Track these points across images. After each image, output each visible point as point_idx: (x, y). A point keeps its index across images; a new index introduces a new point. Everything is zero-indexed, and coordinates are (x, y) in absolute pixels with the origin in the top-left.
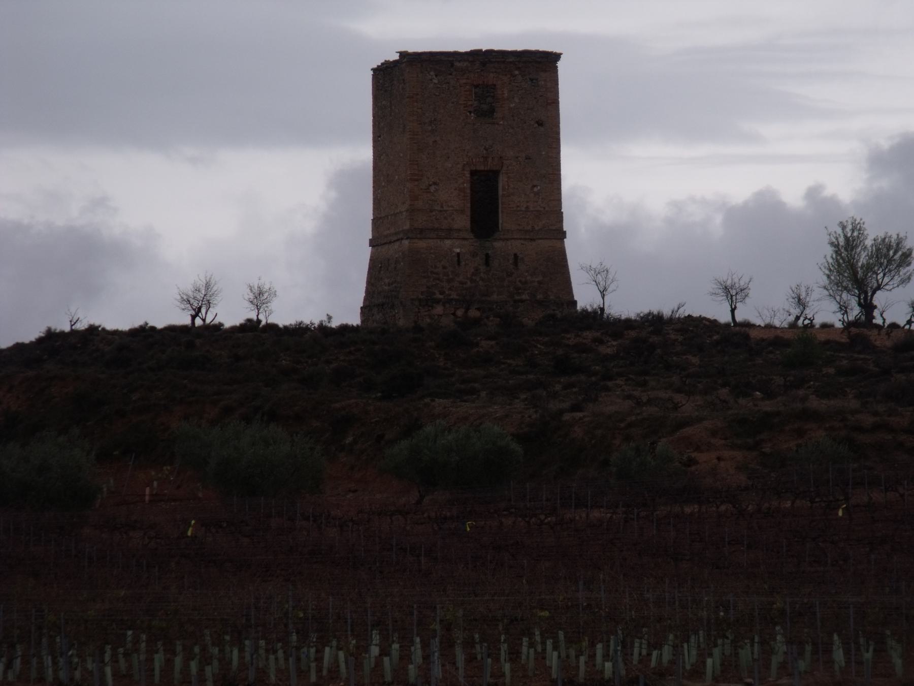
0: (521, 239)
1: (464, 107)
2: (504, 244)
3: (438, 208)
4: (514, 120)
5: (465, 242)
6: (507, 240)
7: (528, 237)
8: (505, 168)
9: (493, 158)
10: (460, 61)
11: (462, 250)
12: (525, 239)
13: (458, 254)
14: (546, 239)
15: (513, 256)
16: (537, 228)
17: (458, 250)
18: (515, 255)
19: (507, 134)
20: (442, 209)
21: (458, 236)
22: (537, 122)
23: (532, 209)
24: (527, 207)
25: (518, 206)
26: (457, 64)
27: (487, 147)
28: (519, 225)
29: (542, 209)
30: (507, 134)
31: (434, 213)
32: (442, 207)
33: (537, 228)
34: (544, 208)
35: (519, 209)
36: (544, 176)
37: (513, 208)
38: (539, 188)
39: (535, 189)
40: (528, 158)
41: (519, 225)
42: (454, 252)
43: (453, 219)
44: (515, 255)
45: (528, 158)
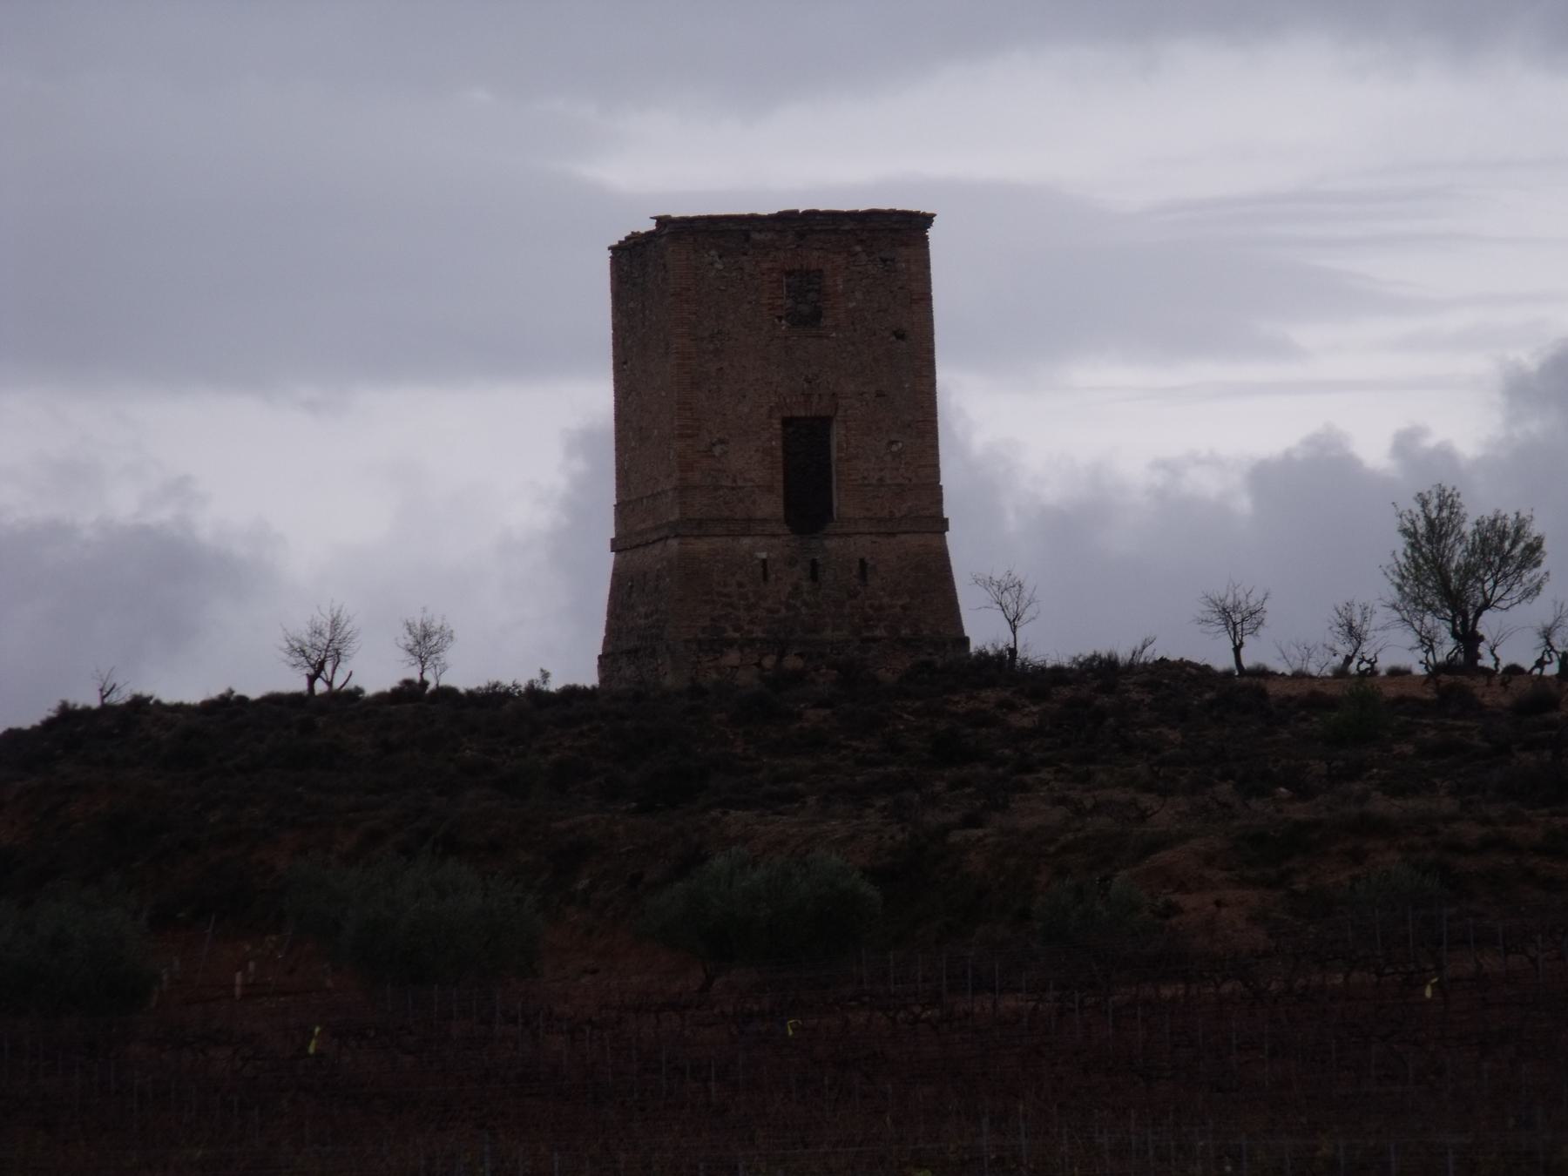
0: (871, 533)
1: (770, 309)
2: (842, 544)
3: (729, 483)
4: (855, 330)
5: (775, 541)
6: (848, 535)
7: (883, 530)
8: (840, 413)
9: (820, 395)
10: (760, 231)
11: (771, 554)
12: (878, 534)
13: (764, 561)
14: (915, 532)
15: (858, 564)
16: (898, 515)
17: (764, 555)
18: (862, 562)
19: (844, 355)
20: (734, 485)
21: (763, 530)
22: (895, 333)
23: (889, 482)
24: (881, 480)
25: (865, 478)
26: (756, 236)
27: (810, 376)
28: (868, 510)
29: (907, 482)
30: (844, 355)
31: (721, 493)
32: (735, 481)
33: (898, 515)
34: (910, 480)
35: (866, 482)
36: (909, 426)
37: (856, 480)
38: (900, 445)
39: (895, 448)
40: (880, 394)
41: (868, 510)
42: (757, 558)
43: (754, 502)
44: (862, 562)
45: (880, 394)
